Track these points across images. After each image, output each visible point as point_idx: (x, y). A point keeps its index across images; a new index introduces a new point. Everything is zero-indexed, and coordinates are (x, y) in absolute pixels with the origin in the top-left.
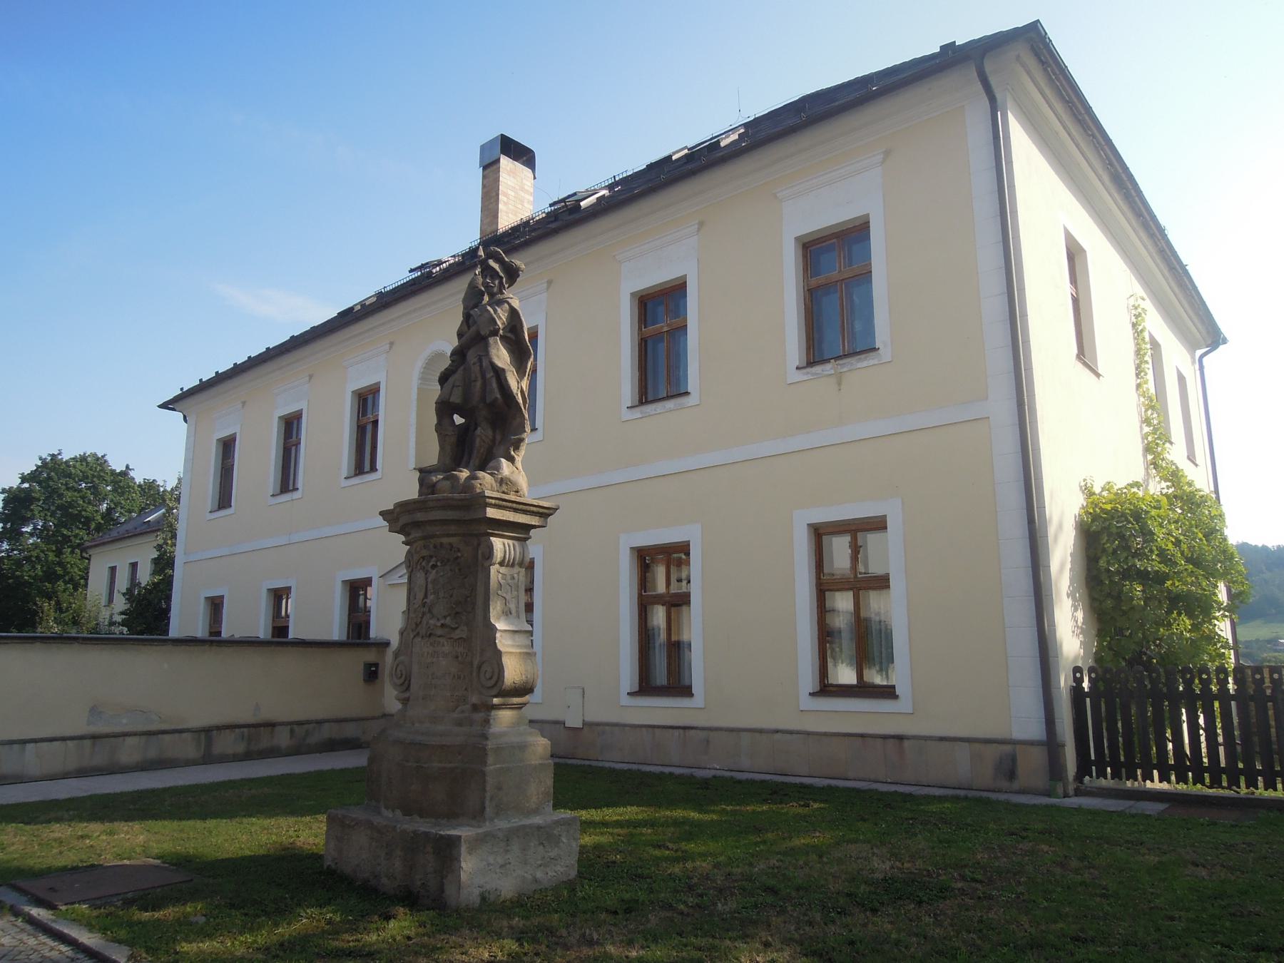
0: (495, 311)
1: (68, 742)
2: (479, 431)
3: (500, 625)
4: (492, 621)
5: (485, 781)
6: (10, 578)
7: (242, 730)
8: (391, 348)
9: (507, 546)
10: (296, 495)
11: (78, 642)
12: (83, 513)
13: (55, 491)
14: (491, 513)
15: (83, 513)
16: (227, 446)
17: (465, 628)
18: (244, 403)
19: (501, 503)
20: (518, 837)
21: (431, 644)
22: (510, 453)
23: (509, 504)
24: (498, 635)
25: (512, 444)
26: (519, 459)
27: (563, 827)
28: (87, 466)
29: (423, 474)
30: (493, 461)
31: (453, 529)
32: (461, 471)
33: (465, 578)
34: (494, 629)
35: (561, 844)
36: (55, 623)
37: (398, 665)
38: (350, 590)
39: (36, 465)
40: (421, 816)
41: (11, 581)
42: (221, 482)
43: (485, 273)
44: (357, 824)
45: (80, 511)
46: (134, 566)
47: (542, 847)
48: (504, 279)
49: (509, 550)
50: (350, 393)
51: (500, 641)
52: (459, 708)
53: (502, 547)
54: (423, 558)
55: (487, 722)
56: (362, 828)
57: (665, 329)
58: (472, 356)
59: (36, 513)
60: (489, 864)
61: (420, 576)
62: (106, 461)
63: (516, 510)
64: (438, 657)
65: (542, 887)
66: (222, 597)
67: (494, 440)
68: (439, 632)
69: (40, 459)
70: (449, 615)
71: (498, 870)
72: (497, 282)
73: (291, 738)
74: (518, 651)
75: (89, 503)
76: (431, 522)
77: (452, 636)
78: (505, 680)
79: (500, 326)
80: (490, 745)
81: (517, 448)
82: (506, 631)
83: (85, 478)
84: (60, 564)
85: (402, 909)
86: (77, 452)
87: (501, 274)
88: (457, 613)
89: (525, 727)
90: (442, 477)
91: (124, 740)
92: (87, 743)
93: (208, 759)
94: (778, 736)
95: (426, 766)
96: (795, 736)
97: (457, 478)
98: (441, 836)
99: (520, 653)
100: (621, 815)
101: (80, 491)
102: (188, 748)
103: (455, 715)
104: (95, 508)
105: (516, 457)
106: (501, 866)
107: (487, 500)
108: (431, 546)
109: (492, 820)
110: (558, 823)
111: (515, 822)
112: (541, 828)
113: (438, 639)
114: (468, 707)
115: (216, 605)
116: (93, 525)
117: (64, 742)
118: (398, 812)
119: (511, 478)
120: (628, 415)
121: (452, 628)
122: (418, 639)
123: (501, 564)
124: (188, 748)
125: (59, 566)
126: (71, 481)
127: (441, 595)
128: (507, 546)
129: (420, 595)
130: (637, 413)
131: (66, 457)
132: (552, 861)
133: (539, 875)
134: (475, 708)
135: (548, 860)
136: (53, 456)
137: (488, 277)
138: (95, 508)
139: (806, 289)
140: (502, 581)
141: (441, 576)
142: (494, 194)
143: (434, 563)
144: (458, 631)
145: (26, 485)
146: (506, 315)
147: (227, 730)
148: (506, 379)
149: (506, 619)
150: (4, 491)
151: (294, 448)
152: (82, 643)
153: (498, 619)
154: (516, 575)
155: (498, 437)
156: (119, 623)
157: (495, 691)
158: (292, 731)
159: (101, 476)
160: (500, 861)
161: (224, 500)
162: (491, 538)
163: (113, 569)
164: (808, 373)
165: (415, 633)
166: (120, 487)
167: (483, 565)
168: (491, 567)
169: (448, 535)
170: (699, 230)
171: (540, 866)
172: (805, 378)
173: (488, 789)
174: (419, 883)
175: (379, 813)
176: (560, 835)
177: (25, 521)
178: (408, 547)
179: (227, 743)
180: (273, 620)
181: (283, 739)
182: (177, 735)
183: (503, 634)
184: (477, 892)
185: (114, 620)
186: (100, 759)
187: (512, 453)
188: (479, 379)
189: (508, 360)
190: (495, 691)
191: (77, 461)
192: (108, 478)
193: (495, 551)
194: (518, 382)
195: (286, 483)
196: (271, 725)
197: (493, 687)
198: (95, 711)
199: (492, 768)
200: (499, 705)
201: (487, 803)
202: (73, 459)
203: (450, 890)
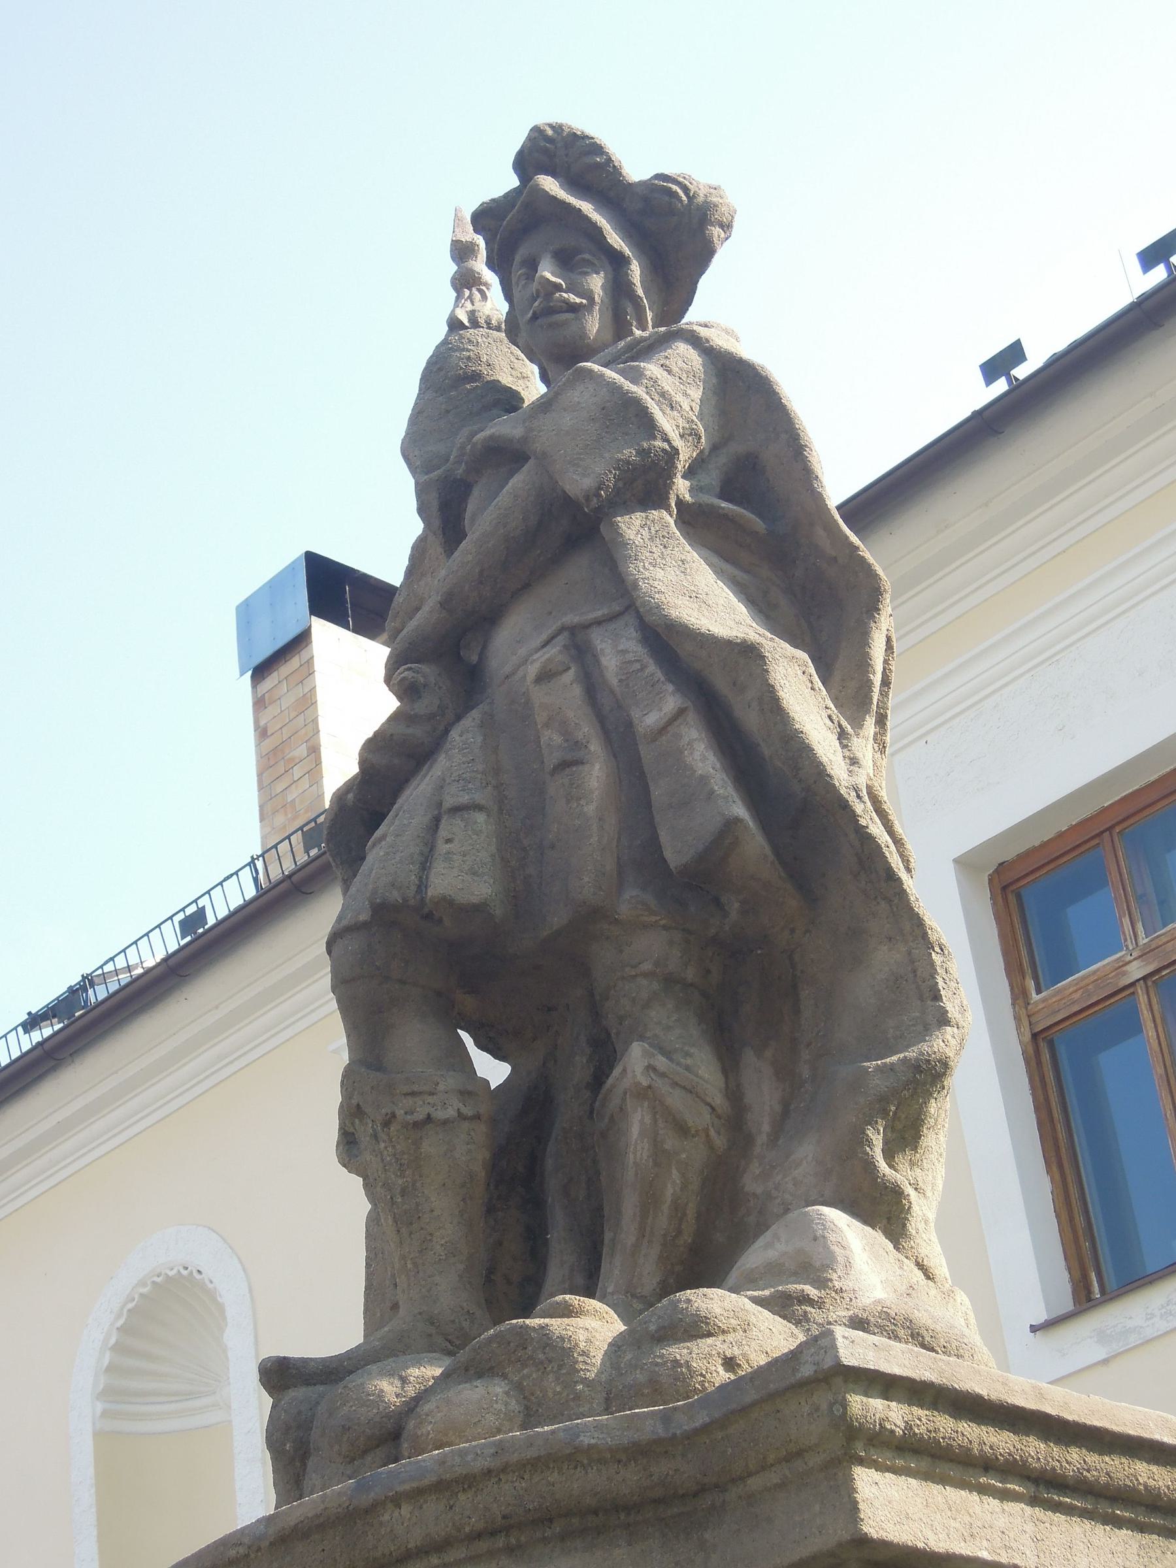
19: (944, 1426)
25: (880, 1107)
29: (298, 1393)
32: (567, 1312)
48: (636, 271)
57: (1136, 971)
72: (597, 283)
79: (678, 443)
87: (615, 239)
90: (438, 1372)
105: (909, 1190)
142: (302, 751)
146: (696, 394)
187: (883, 1166)
188: (595, 746)
194: (842, 735)
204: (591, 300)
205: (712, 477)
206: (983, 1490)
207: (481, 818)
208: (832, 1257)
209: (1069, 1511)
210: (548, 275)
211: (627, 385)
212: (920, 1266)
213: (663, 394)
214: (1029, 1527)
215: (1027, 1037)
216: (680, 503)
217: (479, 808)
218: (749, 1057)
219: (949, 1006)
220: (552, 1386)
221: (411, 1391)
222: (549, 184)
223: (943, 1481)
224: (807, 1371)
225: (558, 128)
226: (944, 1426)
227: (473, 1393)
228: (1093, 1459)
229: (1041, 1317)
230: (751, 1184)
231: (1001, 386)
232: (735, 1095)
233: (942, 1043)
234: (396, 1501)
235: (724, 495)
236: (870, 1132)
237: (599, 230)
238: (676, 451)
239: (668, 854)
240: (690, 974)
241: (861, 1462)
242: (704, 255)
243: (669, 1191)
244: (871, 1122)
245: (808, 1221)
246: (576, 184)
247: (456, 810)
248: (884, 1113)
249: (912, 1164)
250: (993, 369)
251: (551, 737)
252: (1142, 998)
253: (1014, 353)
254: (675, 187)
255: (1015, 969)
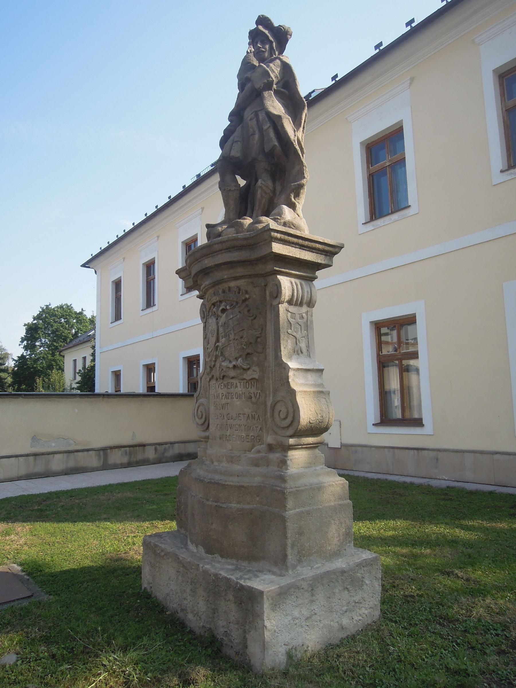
0: (268, 66)
1: (20, 458)
2: (260, 181)
3: (292, 364)
4: (284, 359)
5: (285, 528)
6: (32, 368)
7: (125, 449)
8: (202, 211)
9: (294, 284)
10: (154, 308)
11: (22, 397)
12: (63, 334)
13: (49, 324)
14: (277, 248)
15: (63, 334)
16: (117, 284)
17: (256, 368)
18: (124, 259)
19: (286, 237)
20: (323, 584)
21: (225, 386)
22: (291, 199)
23: (295, 240)
24: (291, 374)
25: (292, 191)
26: (299, 207)
27: (365, 569)
28: (63, 310)
30: (277, 208)
31: (240, 271)
32: (245, 219)
33: (255, 318)
34: (285, 368)
35: (365, 587)
36: (43, 389)
37: (198, 408)
38: (188, 364)
39: (39, 311)
40: (222, 556)
41: (32, 370)
42: (116, 306)
43: (256, 41)
44: (165, 554)
45: (61, 333)
46: (84, 358)
47: (346, 592)
48: (274, 44)
49: (297, 291)
50: (181, 243)
51: (293, 380)
52: (255, 448)
53: (289, 285)
54: (214, 304)
55: (283, 463)
56: (170, 560)
57: (388, 164)
58: (248, 114)
59: (41, 335)
60: (294, 619)
61: (212, 321)
62: (72, 307)
63: (302, 247)
64: (232, 398)
65: (348, 633)
66: (120, 371)
67: (274, 191)
68: (232, 373)
69: (41, 308)
70: (240, 356)
71: (304, 623)
72: (267, 47)
73: (155, 454)
74: (312, 389)
75: (66, 329)
76: (218, 267)
77: (245, 376)
78: (301, 420)
79: (274, 79)
80: (290, 486)
81: (297, 195)
82: (298, 369)
83: (62, 316)
84: (54, 360)
85: (203, 671)
86: (58, 304)
87: (271, 38)
88: (248, 354)
89: (321, 466)
90: (226, 227)
91: (54, 456)
92: (31, 458)
93: (105, 467)
94: (496, 457)
95: (224, 506)
96: (512, 457)
97: (242, 225)
98: (242, 586)
99: (314, 392)
100: (394, 529)
101: (61, 323)
102: (94, 461)
103: (251, 455)
104: (69, 331)
105: (297, 203)
106: (307, 619)
107: (272, 234)
108: (220, 291)
109: (294, 567)
110: (360, 565)
111: (318, 568)
112: (345, 572)
113: (232, 381)
114: (263, 447)
115: (117, 375)
116: (68, 340)
117: (17, 458)
118: (201, 549)
119: (294, 222)
120: (363, 229)
121: (244, 369)
122: (213, 382)
123: (290, 302)
124: (94, 461)
125: (54, 362)
126: (56, 318)
127: (232, 337)
128: (294, 284)
129: (213, 340)
130: (370, 227)
131: (53, 306)
132: (357, 604)
133: (345, 621)
134: (271, 448)
135: (353, 604)
136: (47, 306)
137: (259, 43)
138: (69, 331)
139: (504, 109)
140: (291, 320)
141: (231, 319)
143: (224, 307)
144: (249, 372)
145: (36, 322)
146: (279, 69)
147: (117, 449)
148: (283, 125)
149: (298, 359)
150: (25, 325)
151: (152, 281)
152: (24, 398)
153: (290, 358)
154: (304, 315)
155: (278, 188)
156: (76, 388)
157: (290, 432)
158: (156, 449)
159: (70, 315)
160: (306, 613)
161: (118, 316)
162: (278, 276)
163: (75, 361)
164: (511, 174)
165: (210, 376)
166: (80, 320)
167: (271, 305)
168: (280, 305)
169: (236, 278)
170: (411, 84)
171: (346, 612)
172: (509, 178)
173: (289, 535)
174: (222, 630)
175: (186, 546)
176: (363, 577)
177: (36, 339)
178: (202, 300)
179: (116, 457)
180: (147, 383)
181: (150, 453)
182: (86, 453)
183: (296, 373)
184: (282, 650)
185: (73, 387)
186: (39, 468)
187: (293, 199)
188: (257, 132)
189: (284, 111)
190: (290, 432)
191: (58, 308)
192: (74, 316)
193: (283, 288)
194: (295, 131)
195: (149, 302)
196: (143, 445)
197: (288, 427)
198: (35, 439)
199: (291, 512)
200: (295, 445)
201: (289, 551)
202: (57, 307)
203: (254, 649)
204: (266, 50)
205: (281, 84)
206: (292, 246)
207: (239, 143)
208: (283, 213)
209: (306, 250)
210: (259, 45)
211: (267, 68)
212: (297, 214)
213: (273, 70)
214: (299, 252)
215: (368, 175)
216: (274, 89)
217: (239, 141)
218: (277, 182)
219: (305, 175)
220: (240, 229)
221: (223, 229)
222: (261, 28)
223: (286, 245)
224: (266, 229)
225: (263, 16)
226: (286, 237)
227: (230, 230)
228: (309, 243)
229: (364, 222)
230: (275, 201)
231: (378, 51)
232: (275, 188)
233: (304, 181)
234: (215, 244)
235: (283, 88)
236: (291, 194)
237: (268, 36)
238: (273, 80)
239: (265, 150)
240: (269, 169)
241: (273, 242)
242: (287, 41)
243: (263, 202)
244: (291, 193)
245: (281, 207)
246: (266, 27)
247: (236, 141)
248: (294, 192)
249: (298, 199)
250: (377, 47)
251: (251, 130)
252: (388, 169)
253: (381, 44)
254: (282, 28)
255: (368, 163)
